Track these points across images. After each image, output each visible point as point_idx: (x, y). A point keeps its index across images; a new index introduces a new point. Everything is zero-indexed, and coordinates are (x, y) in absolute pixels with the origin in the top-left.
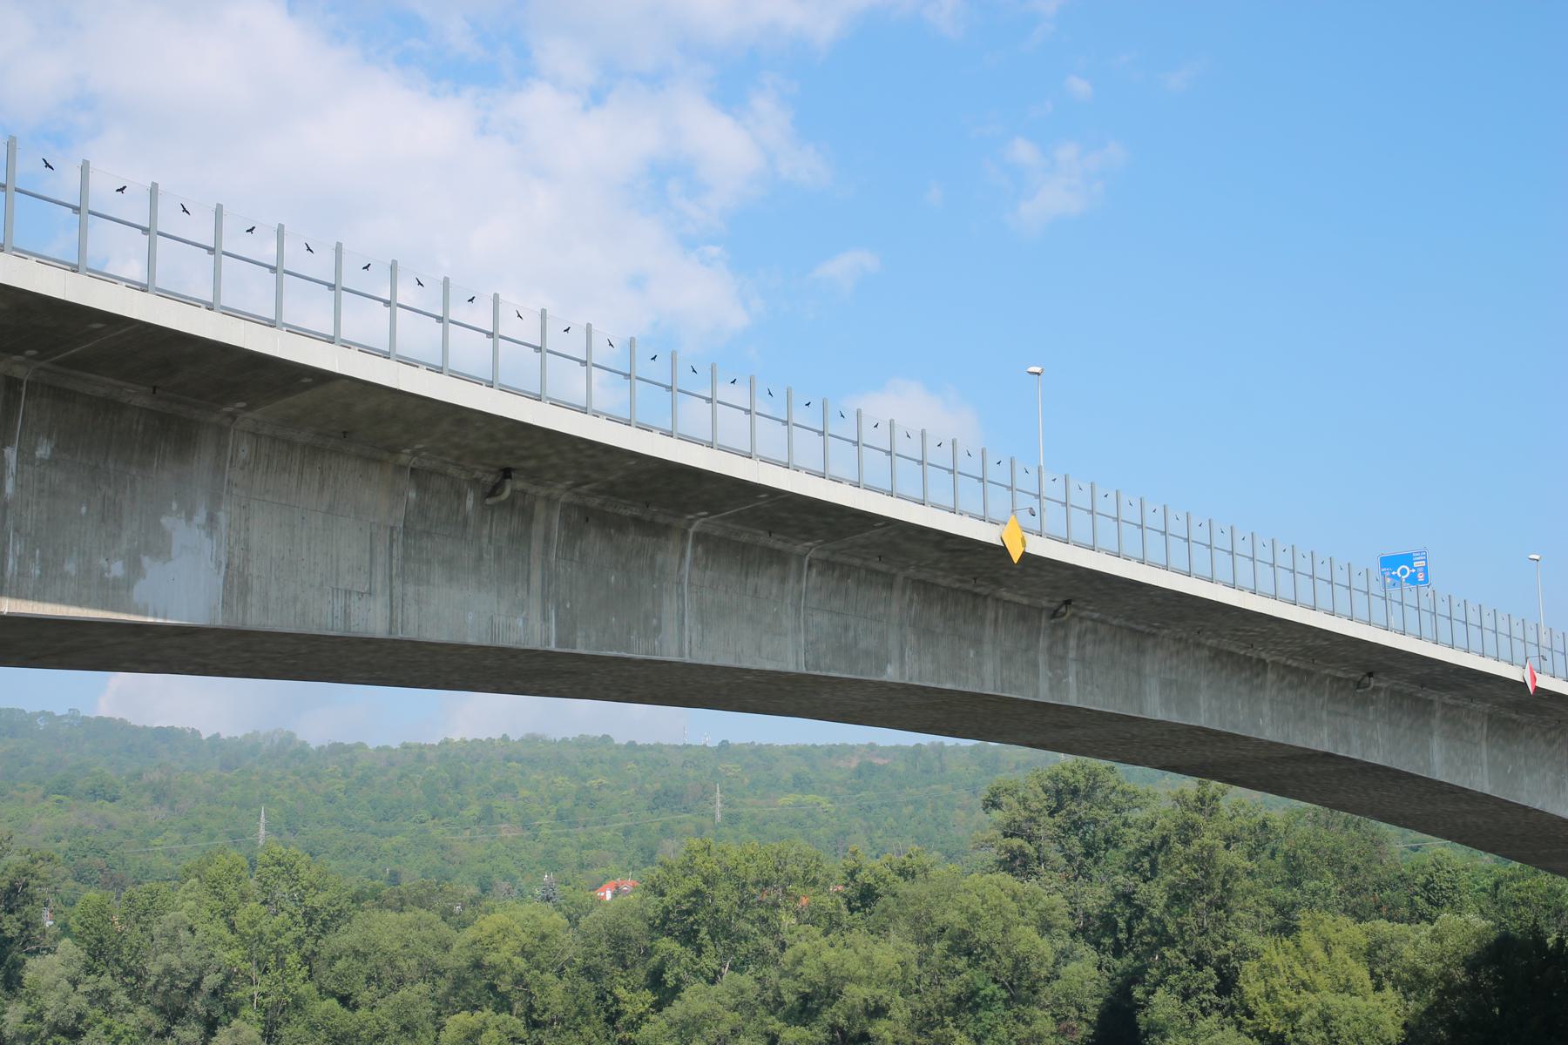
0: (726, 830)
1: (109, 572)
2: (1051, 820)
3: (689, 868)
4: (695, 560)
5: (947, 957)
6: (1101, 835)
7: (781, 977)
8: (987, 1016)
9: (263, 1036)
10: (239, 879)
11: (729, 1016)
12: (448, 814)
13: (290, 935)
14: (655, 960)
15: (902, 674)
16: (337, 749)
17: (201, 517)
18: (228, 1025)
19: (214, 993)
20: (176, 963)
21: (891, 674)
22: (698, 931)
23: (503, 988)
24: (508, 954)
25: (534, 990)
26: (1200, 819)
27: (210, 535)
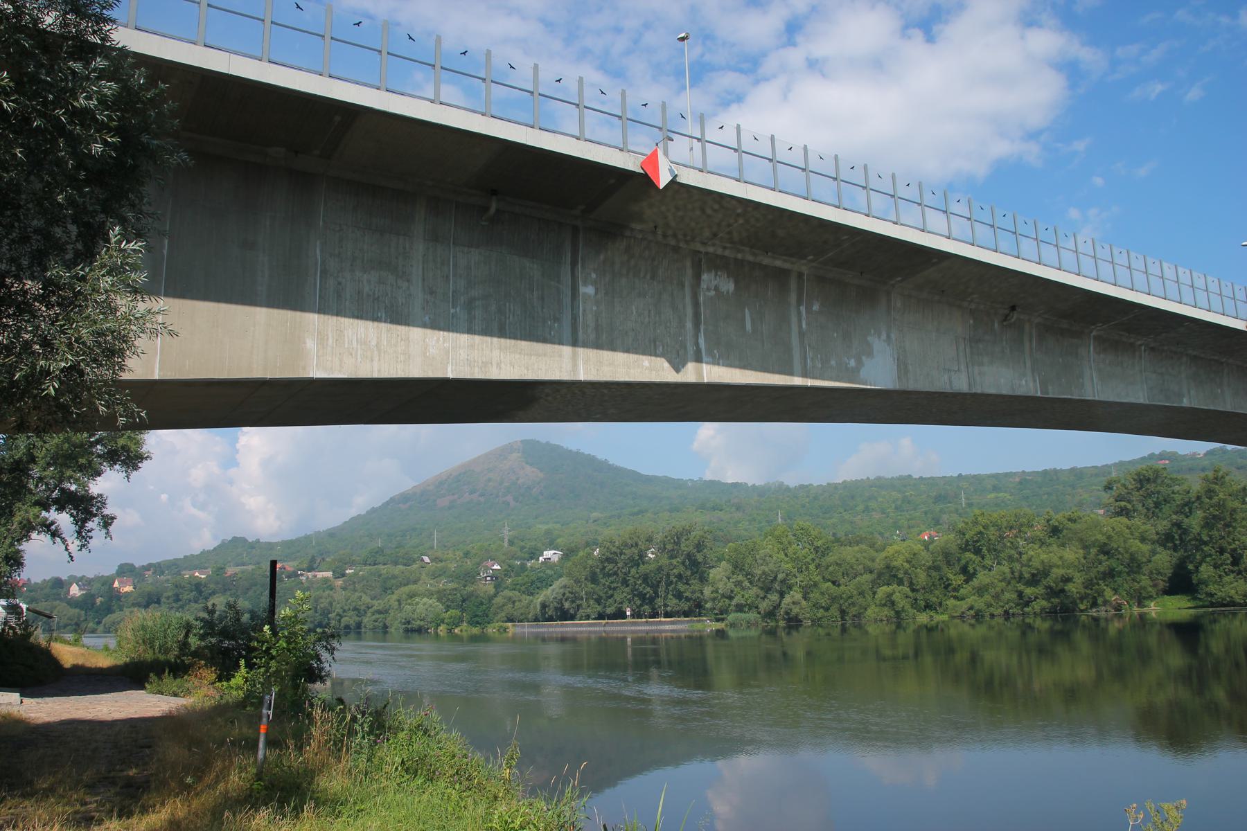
0: (968, 510)
1: (849, 364)
2: (1137, 493)
3: (975, 523)
4: (1094, 348)
5: (1098, 555)
6: (1161, 498)
7: (1022, 567)
8: (1119, 580)
9: (803, 598)
10: (787, 536)
11: (1000, 584)
12: (851, 509)
13: (810, 557)
14: (963, 562)
15: (1191, 403)
16: (802, 487)
17: (884, 336)
18: (789, 593)
19: (781, 582)
20: (767, 570)
21: (1186, 403)
22: (982, 549)
23: (900, 576)
24: (901, 562)
25: (913, 576)
26: (1217, 488)
27: (889, 345)
